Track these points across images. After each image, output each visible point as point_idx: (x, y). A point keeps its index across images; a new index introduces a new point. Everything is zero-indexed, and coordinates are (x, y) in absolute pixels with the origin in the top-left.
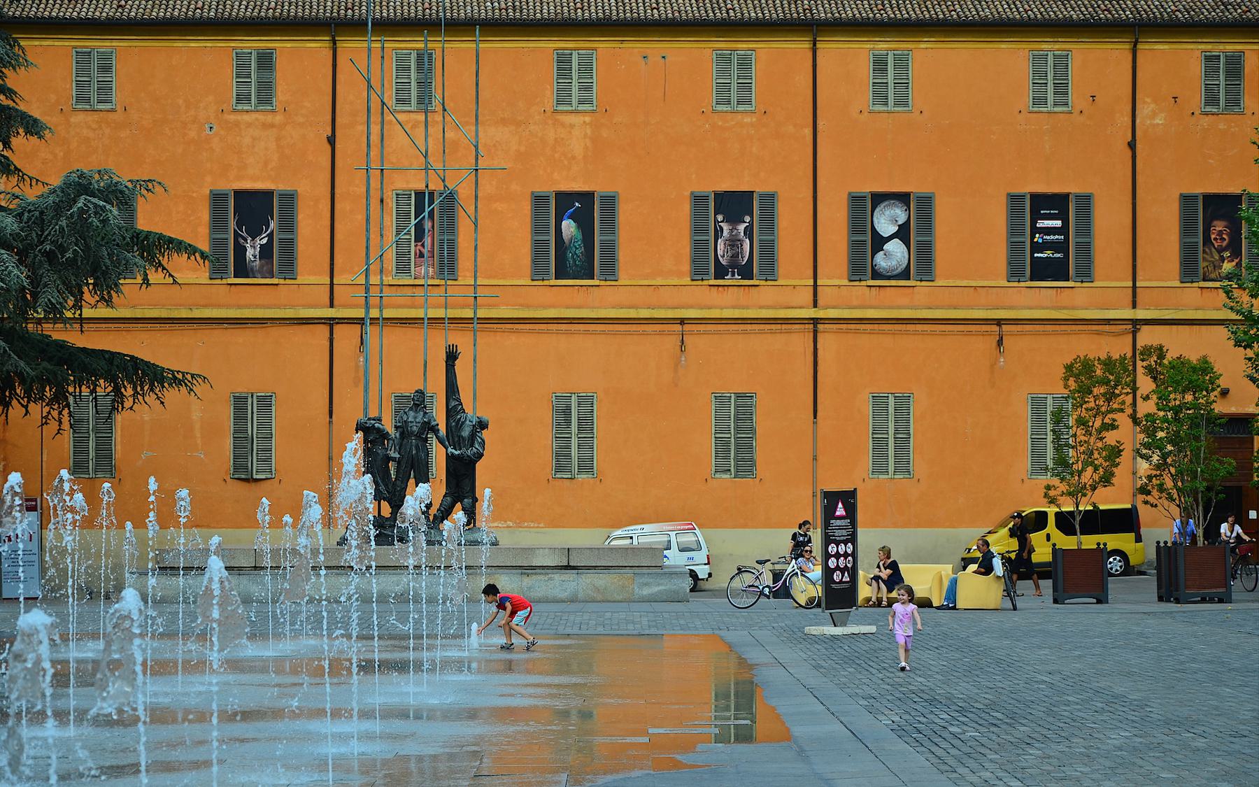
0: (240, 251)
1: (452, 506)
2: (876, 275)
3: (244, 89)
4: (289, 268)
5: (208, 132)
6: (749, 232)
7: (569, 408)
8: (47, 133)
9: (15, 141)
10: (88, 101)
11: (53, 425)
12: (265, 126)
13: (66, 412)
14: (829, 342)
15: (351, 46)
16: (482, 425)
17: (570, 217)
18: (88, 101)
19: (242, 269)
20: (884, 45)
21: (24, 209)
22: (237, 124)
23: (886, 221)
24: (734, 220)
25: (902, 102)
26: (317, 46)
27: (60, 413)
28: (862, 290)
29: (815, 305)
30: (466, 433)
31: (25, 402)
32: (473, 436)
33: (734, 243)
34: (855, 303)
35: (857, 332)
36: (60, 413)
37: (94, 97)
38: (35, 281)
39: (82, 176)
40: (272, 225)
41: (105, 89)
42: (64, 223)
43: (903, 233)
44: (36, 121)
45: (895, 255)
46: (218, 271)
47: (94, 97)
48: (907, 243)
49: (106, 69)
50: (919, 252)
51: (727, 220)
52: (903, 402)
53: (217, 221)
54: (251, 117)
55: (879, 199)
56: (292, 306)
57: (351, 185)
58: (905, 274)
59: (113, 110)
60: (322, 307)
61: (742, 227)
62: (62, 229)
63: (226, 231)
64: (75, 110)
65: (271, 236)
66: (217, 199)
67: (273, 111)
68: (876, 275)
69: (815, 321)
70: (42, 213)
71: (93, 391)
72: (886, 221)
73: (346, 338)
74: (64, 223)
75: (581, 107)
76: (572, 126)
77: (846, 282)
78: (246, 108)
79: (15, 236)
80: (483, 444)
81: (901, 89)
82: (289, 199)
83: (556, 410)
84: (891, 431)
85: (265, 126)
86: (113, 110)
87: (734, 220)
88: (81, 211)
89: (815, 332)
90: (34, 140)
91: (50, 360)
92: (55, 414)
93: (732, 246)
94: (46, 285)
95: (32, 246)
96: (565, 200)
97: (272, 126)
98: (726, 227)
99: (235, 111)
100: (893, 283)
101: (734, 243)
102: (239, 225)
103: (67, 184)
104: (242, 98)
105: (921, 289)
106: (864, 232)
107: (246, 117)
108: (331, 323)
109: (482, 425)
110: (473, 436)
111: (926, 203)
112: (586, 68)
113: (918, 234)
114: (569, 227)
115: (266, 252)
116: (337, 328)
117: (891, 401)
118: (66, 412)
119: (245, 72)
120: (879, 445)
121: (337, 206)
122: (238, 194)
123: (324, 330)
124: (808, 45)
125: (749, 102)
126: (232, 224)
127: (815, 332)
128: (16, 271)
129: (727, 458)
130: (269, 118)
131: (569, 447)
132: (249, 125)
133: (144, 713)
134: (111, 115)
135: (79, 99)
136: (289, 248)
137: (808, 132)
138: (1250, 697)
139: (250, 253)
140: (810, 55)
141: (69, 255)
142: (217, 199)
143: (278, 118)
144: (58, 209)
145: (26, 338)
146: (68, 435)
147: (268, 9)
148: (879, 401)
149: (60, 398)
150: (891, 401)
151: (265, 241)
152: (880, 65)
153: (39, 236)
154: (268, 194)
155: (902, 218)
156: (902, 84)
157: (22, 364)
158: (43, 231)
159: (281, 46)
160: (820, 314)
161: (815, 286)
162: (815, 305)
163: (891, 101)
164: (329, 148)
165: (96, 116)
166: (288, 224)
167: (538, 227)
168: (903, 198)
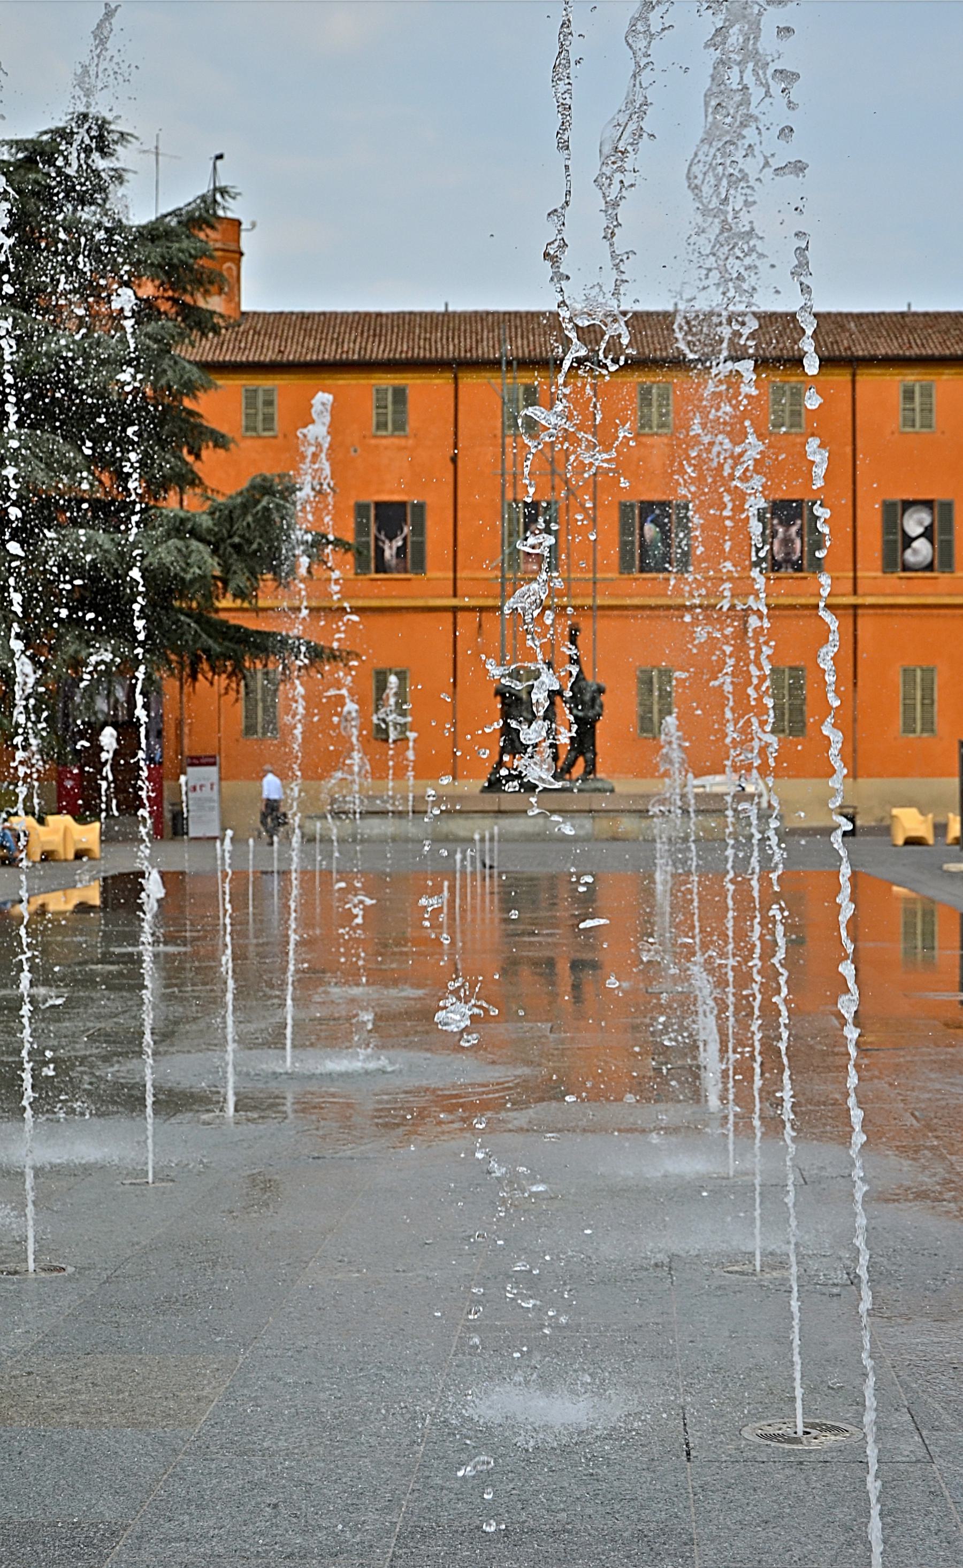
0: (380, 551)
1: (576, 758)
2: (906, 568)
3: (382, 419)
4: (419, 565)
5: (352, 453)
6: (800, 533)
7: (651, 678)
8: (232, 446)
9: (204, 454)
10: (255, 429)
11: (232, 694)
12: (401, 449)
13: (242, 683)
14: (866, 624)
15: (471, 381)
16: (601, 690)
17: (652, 521)
18: (255, 429)
19: (382, 567)
20: (912, 377)
21: (216, 509)
22: (377, 446)
23: (914, 523)
24: (787, 524)
25: (927, 425)
26: (440, 382)
27: (238, 685)
28: (894, 579)
29: (855, 592)
30: (587, 697)
31: (210, 675)
32: (593, 700)
33: (787, 541)
34: (888, 591)
35: (890, 615)
36: (238, 685)
37: (260, 426)
38: (226, 568)
39: (265, 479)
40: (406, 530)
41: (268, 420)
42: (250, 518)
43: (928, 533)
44: (223, 436)
45: (922, 550)
46: (361, 566)
47: (260, 426)
48: (931, 541)
49: (269, 403)
50: (941, 549)
51: (781, 523)
52: (928, 672)
53: (361, 529)
54: (388, 441)
55: (907, 505)
56: (422, 597)
57: (469, 497)
58: (930, 567)
59: (275, 437)
60: (447, 597)
61: (794, 530)
62: (248, 524)
63: (368, 534)
64: (244, 437)
65: (405, 539)
66: (361, 509)
67: (406, 437)
68: (906, 568)
69: (855, 607)
70: (231, 512)
71: (265, 666)
72: (914, 523)
73: (467, 622)
74: (250, 518)
75: (660, 431)
76: (652, 446)
77: (879, 574)
78: (384, 433)
79: (209, 531)
80: (601, 706)
81: (926, 413)
82: (420, 508)
83: (641, 681)
84: (919, 696)
85: (401, 449)
86: (275, 437)
87: (787, 524)
88: (266, 509)
89: (855, 616)
90: (221, 452)
91: (231, 640)
92: (234, 685)
93: (786, 545)
94: (235, 572)
95: (223, 540)
96: (647, 508)
97: (405, 448)
98: (781, 530)
99: (375, 437)
100: (920, 574)
101: (787, 541)
102: (379, 530)
103: (253, 487)
104: (381, 425)
105: (944, 578)
106: (895, 533)
107: (384, 442)
108: (455, 610)
109: (601, 690)
110: (593, 700)
111: (947, 508)
112: (664, 396)
113: (941, 533)
114: (650, 530)
115: (401, 551)
116: (460, 615)
117: (919, 673)
118: (242, 683)
119: (383, 403)
120: (909, 709)
121: (460, 515)
122: (378, 505)
123: (449, 616)
124: (849, 378)
125: (800, 426)
126: (373, 529)
127: (855, 616)
128: (210, 560)
129: (783, 720)
130: (403, 442)
131: (651, 712)
132: (386, 448)
133: (717, 993)
134: (273, 441)
135: (247, 429)
136: (420, 549)
137: (849, 449)
138: (487, 879)
139: (388, 554)
140: (850, 386)
141: (255, 546)
142: (361, 509)
143: (411, 442)
144: (245, 507)
145: (209, 621)
146: (241, 705)
147: (401, 352)
148: (908, 673)
149: (238, 671)
150: (919, 673)
151: (400, 543)
152: (909, 395)
153: (229, 532)
154: (403, 504)
155: (927, 522)
156: (927, 410)
157: (210, 642)
158: (232, 526)
159: (411, 382)
160: (859, 601)
161: (855, 578)
162: (855, 592)
163: (918, 423)
164: (451, 466)
165: (260, 442)
166: (419, 529)
167: (626, 528)
168: (928, 504)
